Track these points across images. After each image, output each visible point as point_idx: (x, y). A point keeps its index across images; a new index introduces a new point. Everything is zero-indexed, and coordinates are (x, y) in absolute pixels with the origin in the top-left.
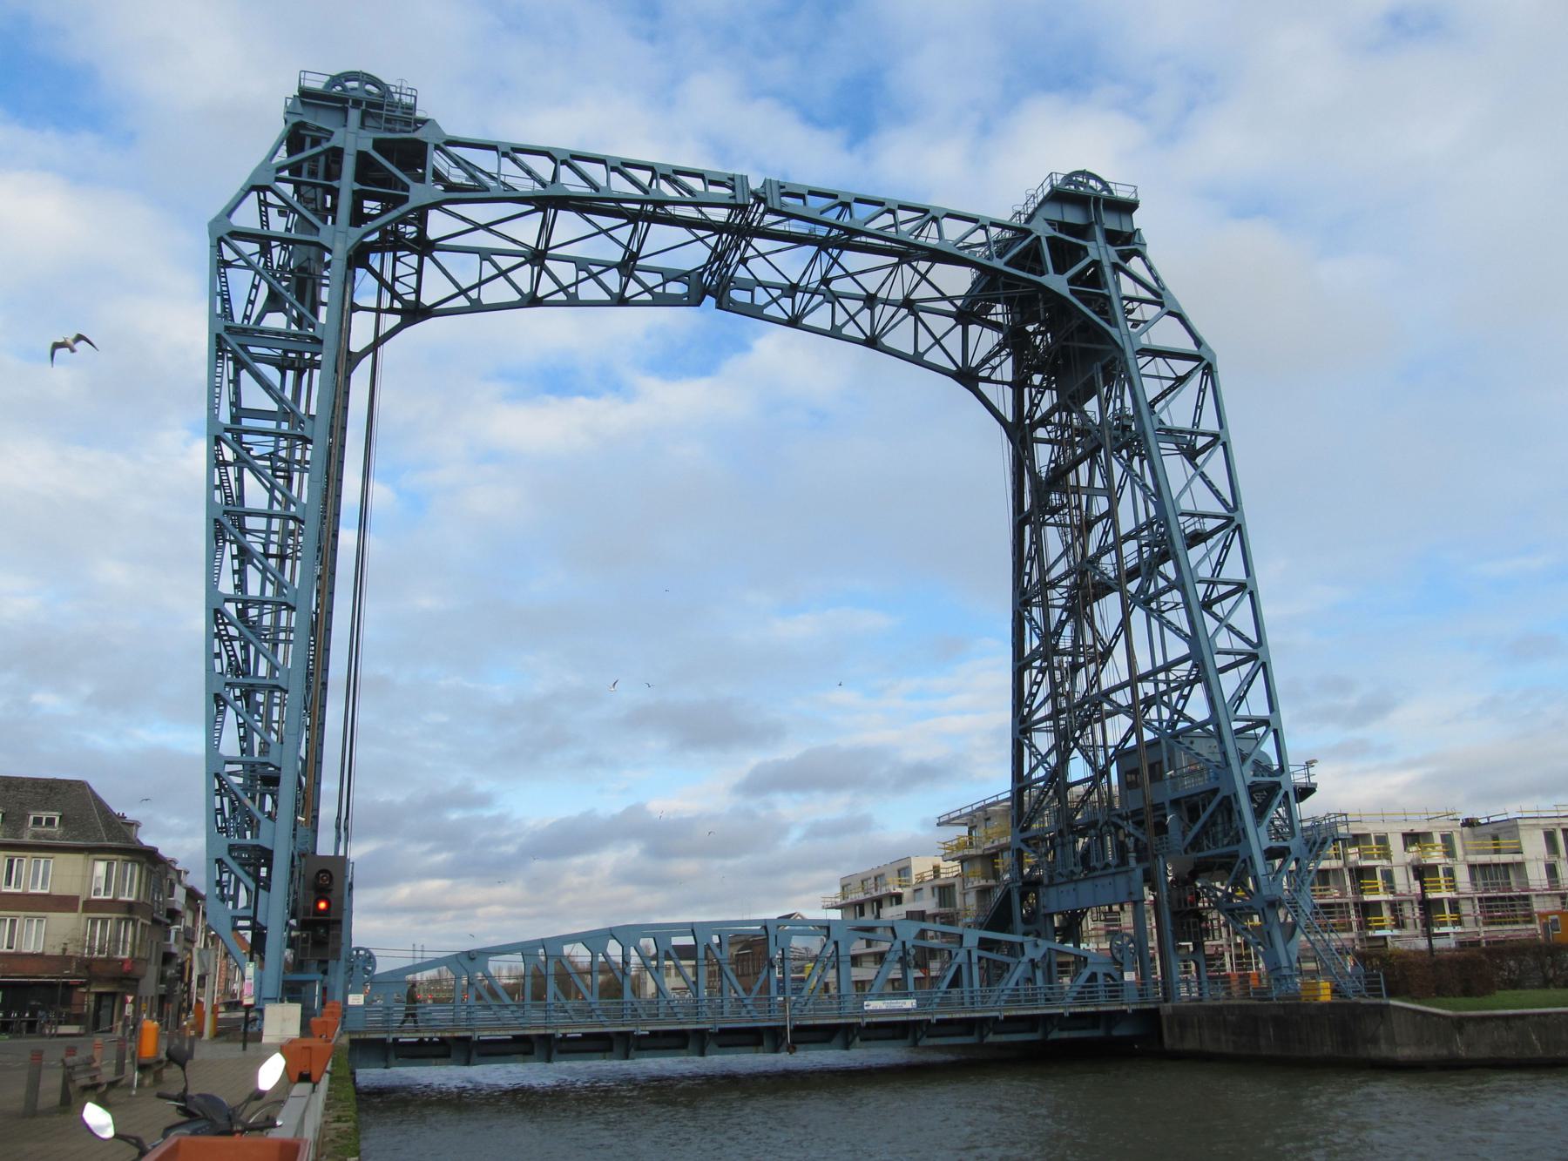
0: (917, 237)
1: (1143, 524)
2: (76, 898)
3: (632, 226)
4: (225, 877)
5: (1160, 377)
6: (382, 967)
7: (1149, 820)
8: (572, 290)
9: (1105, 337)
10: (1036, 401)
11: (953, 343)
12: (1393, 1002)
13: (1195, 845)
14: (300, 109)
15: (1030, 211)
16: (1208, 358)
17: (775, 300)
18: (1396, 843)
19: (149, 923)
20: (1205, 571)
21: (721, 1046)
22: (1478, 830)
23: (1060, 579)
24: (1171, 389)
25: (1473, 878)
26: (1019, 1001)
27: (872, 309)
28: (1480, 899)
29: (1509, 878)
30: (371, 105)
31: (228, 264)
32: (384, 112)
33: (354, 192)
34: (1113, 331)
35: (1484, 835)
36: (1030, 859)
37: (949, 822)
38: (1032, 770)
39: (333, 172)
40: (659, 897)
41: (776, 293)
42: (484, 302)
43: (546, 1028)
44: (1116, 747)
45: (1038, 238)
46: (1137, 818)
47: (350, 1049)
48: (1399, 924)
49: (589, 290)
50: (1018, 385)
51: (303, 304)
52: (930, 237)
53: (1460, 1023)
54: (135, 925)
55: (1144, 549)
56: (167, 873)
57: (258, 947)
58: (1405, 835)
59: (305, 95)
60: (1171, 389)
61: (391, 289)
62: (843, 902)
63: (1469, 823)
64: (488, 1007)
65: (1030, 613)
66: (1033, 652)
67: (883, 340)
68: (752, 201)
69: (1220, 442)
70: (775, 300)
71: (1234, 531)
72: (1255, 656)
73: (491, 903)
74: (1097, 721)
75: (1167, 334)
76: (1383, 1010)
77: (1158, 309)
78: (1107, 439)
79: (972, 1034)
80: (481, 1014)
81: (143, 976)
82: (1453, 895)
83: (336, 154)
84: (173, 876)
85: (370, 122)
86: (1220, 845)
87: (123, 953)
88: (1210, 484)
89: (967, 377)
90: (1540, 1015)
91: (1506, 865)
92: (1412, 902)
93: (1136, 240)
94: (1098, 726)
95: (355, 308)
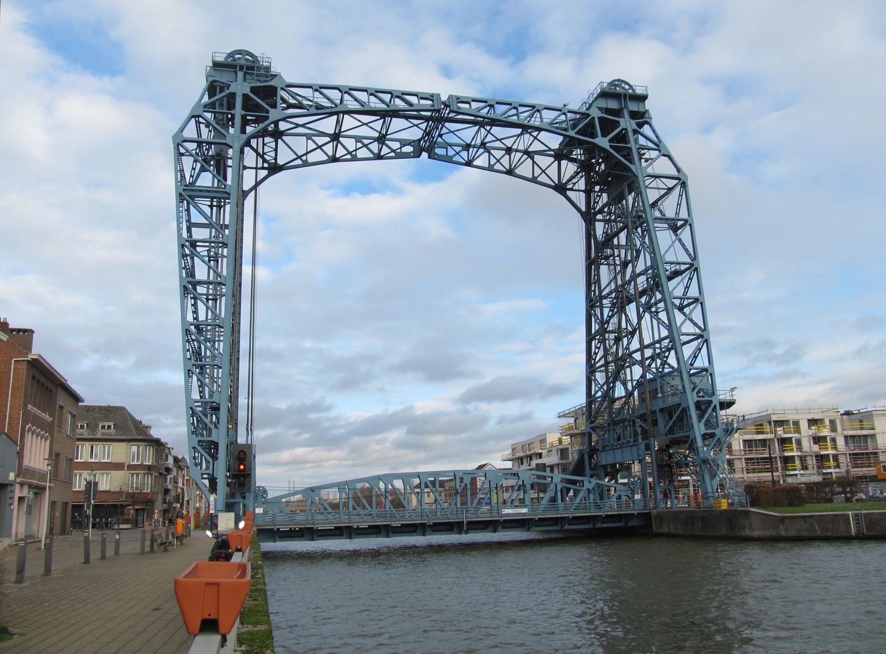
0: (528, 122)
1: (649, 267)
2: (124, 464)
3: (383, 120)
4: (196, 455)
5: (658, 188)
6: (271, 495)
7: (649, 418)
8: (354, 153)
9: (628, 169)
10: (597, 201)
11: (553, 172)
12: (752, 509)
13: (671, 431)
14: (213, 73)
15: (591, 102)
16: (683, 179)
17: (458, 153)
18: (804, 425)
19: (158, 475)
20: (679, 292)
21: (433, 531)
22: (852, 417)
23: (608, 294)
24: (666, 194)
25: (846, 443)
26: (586, 509)
27: (510, 155)
28: (850, 454)
29: (867, 443)
30: (249, 68)
31: (182, 155)
32: (255, 72)
33: (242, 116)
34: (632, 167)
35: (855, 420)
36: (594, 437)
37: (564, 416)
38: (596, 392)
39: (231, 106)
40: (412, 455)
41: (458, 149)
42: (309, 162)
43: (349, 523)
44: (638, 380)
45: (593, 118)
46: (643, 417)
47: (257, 534)
48: (804, 467)
49: (363, 153)
50: (588, 192)
51: (219, 175)
52: (536, 121)
53: (782, 520)
54: (151, 476)
55: (650, 280)
56: (164, 450)
57: (213, 488)
58: (809, 420)
59: (216, 65)
60: (666, 194)
61: (262, 157)
62: (512, 458)
63: (848, 413)
64: (322, 513)
65: (595, 311)
66: (596, 332)
67: (516, 171)
68: (442, 106)
69: (688, 224)
70: (458, 153)
71: (694, 270)
72: (702, 336)
73: (330, 459)
74: (627, 367)
75: (662, 166)
76: (747, 513)
77: (657, 152)
78: (630, 223)
79: (557, 525)
80: (319, 517)
81: (156, 501)
82: (835, 452)
83: (233, 96)
84: (167, 451)
85: (248, 77)
86: (685, 431)
87: (147, 490)
88: (683, 245)
89: (561, 188)
90: (819, 516)
91: (865, 436)
92: (812, 456)
93: (646, 116)
94: (628, 370)
95: (245, 168)
